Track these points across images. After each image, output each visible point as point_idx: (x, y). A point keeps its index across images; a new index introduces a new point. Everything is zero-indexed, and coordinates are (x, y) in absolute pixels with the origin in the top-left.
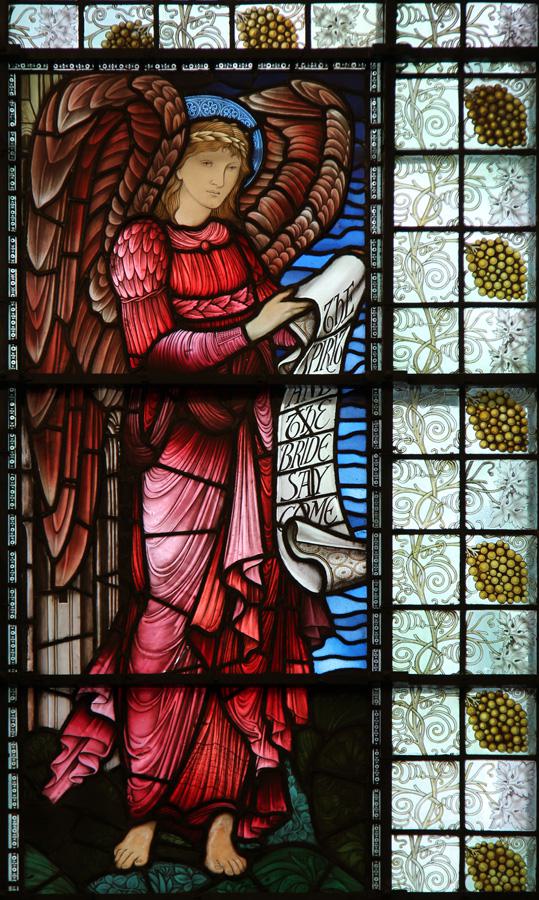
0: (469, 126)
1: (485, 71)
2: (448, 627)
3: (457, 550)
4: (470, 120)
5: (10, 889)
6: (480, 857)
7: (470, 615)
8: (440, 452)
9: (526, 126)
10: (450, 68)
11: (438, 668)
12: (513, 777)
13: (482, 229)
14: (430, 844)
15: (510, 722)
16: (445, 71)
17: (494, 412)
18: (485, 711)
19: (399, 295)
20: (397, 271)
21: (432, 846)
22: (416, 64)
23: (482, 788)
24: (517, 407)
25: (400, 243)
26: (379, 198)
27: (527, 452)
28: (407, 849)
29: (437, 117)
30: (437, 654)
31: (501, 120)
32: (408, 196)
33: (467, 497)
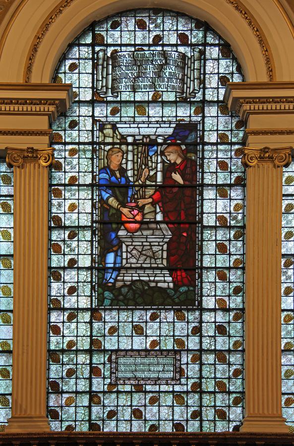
0: (219, 112)
28: (205, 410)
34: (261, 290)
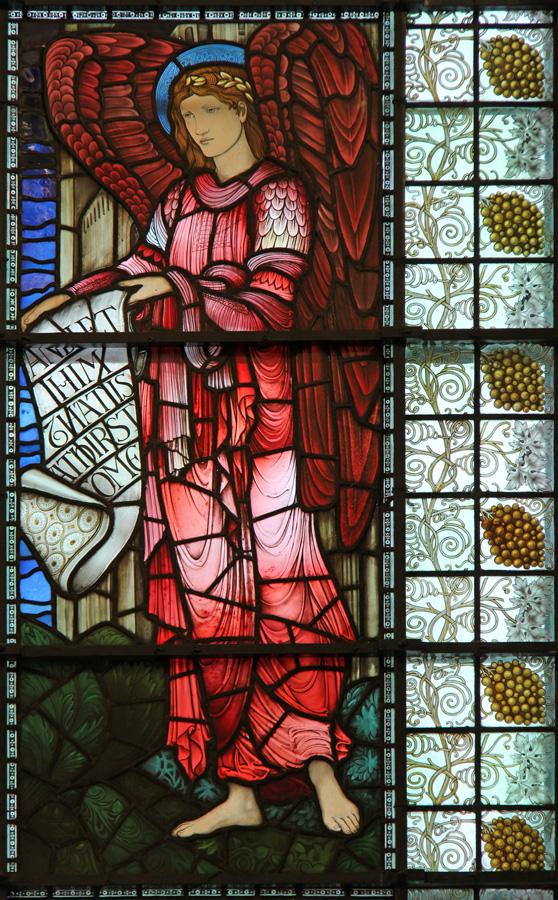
1: (501, 22)
2: (462, 124)
3: (473, 826)
4: (486, 228)
5: (8, 327)
6: (497, 833)
7: (486, 737)
8: (454, 256)
9: (543, 77)
10: (465, 19)
11: (453, 635)
12: (528, 280)
13: (499, 495)
14: (444, 39)
15: (527, 692)
16: (459, 22)
17: (509, 370)
18: (499, 55)
19: (412, 252)
20: (410, 696)
21: (446, 823)
22: (430, 12)
23: (499, 761)
24: (534, 365)
25: (413, 42)
26: (392, 216)
27: (543, 412)
29: (453, 226)
30: (451, 467)
31: (519, 696)
32: (422, 150)
33: (481, 302)
34: (74, 382)
